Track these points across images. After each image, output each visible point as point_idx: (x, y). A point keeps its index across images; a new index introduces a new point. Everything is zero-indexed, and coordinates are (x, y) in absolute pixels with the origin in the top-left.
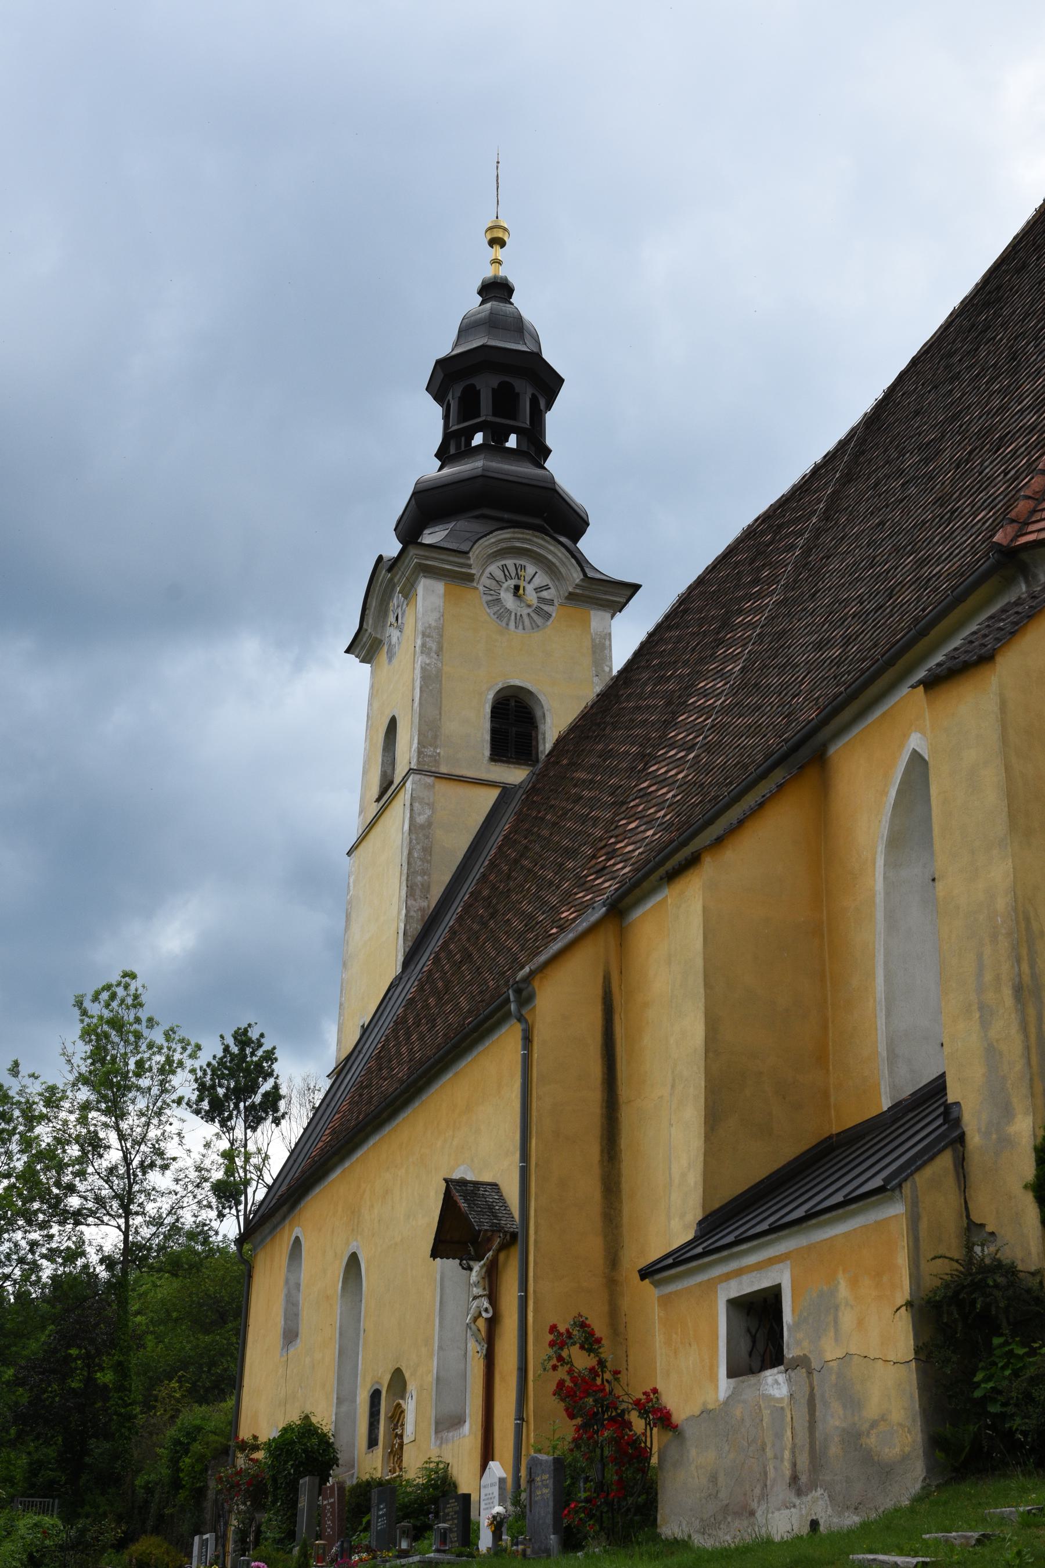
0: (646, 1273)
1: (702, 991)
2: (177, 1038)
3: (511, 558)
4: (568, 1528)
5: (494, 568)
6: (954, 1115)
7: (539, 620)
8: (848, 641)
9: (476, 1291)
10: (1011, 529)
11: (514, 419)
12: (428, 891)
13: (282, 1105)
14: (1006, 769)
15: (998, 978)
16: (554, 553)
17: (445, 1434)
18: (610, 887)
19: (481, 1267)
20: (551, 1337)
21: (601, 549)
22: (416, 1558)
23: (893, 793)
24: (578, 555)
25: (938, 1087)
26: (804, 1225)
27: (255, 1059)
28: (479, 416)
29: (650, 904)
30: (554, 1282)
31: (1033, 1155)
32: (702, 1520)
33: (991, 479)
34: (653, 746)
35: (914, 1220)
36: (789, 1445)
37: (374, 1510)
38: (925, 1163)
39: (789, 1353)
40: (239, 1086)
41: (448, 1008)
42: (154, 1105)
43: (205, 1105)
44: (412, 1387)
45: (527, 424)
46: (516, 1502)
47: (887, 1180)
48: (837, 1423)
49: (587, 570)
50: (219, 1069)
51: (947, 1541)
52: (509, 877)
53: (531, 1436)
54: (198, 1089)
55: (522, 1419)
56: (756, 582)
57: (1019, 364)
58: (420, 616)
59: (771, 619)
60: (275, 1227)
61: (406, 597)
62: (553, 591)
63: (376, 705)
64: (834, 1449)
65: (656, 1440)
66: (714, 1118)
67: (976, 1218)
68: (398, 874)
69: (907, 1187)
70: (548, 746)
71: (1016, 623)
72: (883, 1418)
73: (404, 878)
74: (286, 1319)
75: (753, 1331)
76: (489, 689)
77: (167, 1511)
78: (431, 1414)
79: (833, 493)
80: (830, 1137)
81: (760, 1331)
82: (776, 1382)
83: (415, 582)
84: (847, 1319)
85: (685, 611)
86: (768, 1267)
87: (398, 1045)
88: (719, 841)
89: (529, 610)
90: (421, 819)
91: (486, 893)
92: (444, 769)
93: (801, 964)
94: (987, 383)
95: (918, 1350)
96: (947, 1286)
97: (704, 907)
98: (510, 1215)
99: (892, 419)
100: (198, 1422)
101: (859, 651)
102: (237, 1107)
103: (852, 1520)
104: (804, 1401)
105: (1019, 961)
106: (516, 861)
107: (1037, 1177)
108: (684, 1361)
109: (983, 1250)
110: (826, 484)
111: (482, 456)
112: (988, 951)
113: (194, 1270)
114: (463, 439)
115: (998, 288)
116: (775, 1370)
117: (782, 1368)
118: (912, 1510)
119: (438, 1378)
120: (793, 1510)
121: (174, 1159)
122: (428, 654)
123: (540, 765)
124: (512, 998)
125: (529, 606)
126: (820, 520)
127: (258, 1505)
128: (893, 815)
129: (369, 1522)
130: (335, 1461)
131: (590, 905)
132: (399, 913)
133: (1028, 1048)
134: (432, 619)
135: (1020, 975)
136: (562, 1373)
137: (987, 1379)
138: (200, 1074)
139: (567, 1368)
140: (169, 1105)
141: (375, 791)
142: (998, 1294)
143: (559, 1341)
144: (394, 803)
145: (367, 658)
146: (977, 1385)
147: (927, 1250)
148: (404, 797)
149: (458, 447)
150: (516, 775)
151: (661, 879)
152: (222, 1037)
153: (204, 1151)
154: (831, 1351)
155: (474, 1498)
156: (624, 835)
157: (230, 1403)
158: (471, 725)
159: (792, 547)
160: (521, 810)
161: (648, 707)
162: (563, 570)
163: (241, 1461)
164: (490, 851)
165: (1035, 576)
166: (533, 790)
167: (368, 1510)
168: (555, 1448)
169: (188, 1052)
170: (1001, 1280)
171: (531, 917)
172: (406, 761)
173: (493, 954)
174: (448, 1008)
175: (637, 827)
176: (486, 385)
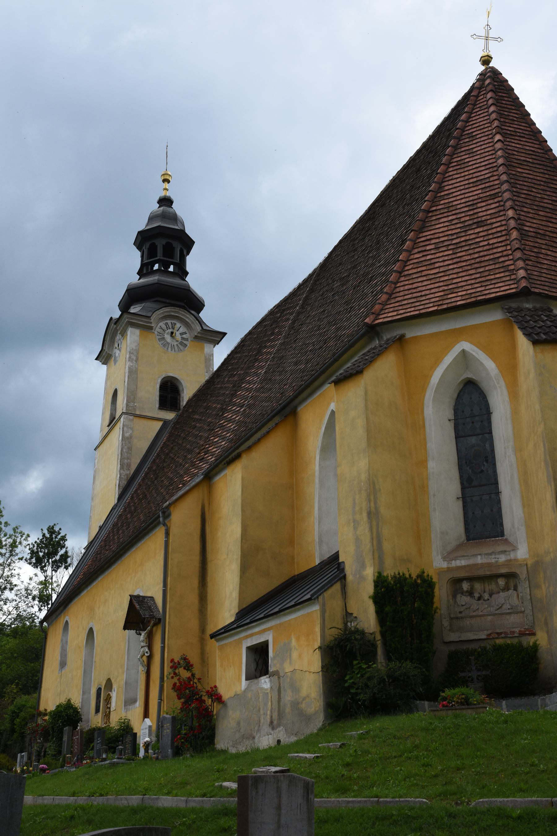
0: (213, 636)
1: (240, 513)
2: (19, 531)
3: (170, 320)
4: (177, 747)
5: (162, 324)
6: (342, 567)
7: (182, 347)
8: (308, 361)
9: (143, 644)
10: (372, 317)
11: (172, 258)
12: (130, 467)
13: (69, 560)
14: (367, 421)
15: (361, 509)
16: (189, 318)
17: (128, 707)
18: (205, 466)
19: (145, 634)
20: (171, 664)
21: (210, 317)
22: (108, 762)
23: (323, 428)
24: (199, 319)
25: (336, 556)
26: (279, 615)
27: (57, 540)
28: (157, 257)
29: (222, 474)
30: (177, 639)
31: (373, 584)
32: (233, 741)
33: (367, 294)
34: (226, 405)
35: (323, 612)
36: (270, 709)
37: (95, 741)
38: (328, 588)
39: (271, 670)
40: (49, 551)
41: (135, 519)
42: (7, 561)
43: (34, 560)
44: (115, 686)
45: (178, 261)
46: (158, 736)
47: (312, 596)
48: (289, 699)
49: (203, 326)
50: (40, 545)
51: (328, 746)
52: (164, 461)
53: (165, 707)
54: (30, 553)
55: (161, 700)
56: (272, 334)
57: (380, 246)
58: (128, 344)
59: (278, 350)
60: (57, 616)
61: (122, 336)
62: (188, 335)
63: (108, 384)
64: (288, 710)
65: (216, 708)
66: (244, 568)
67: (349, 611)
68: (116, 459)
69: (321, 598)
70: (185, 403)
71: (373, 357)
72: (308, 696)
73: (119, 461)
74: (61, 657)
75: (257, 660)
76: (159, 378)
77: (9, 743)
78: (123, 698)
79: (306, 297)
80: (294, 576)
81: (260, 660)
82: (265, 682)
83: (126, 329)
84: (295, 654)
85: (243, 346)
86: (263, 633)
87: (114, 535)
88: (250, 448)
89: (177, 343)
90: (127, 435)
91: (154, 468)
92: (138, 413)
93: (286, 496)
94: (368, 253)
95: (323, 667)
96: (335, 639)
97: (242, 477)
98: (158, 610)
99: (330, 266)
100: (23, 703)
101: (311, 366)
102: (48, 561)
103: (293, 739)
104: (276, 690)
105: (370, 501)
106: (167, 454)
107: (374, 593)
108: (229, 675)
109: (351, 625)
110: (303, 292)
111: (158, 274)
112: (357, 497)
113: (24, 635)
114: (150, 267)
115: (374, 213)
116: (265, 677)
117: (268, 676)
118: (317, 734)
119: (126, 683)
120: (270, 736)
121: (15, 585)
122: (132, 362)
123: (181, 412)
124: (161, 515)
125: (177, 341)
126: (300, 308)
127: (46, 740)
128: (324, 438)
129: (93, 746)
130: (80, 720)
131: (196, 475)
132: (117, 476)
133: (372, 539)
134: (134, 346)
135: (370, 507)
136: (175, 680)
137: (350, 679)
138: (31, 546)
139: (178, 677)
140: (14, 562)
141: (107, 422)
142: (356, 642)
143: (175, 666)
144: (116, 427)
145: (104, 363)
146: (346, 681)
147: (328, 625)
148: (120, 425)
149: (147, 270)
150: (170, 416)
151: (225, 464)
152: (42, 530)
153: (29, 582)
154: (288, 668)
155: (138, 735)
156: (213, 444)
157: (36, 695)
158: (151, 393)
159: (288, 320)
160: (171, 431)
161: (226, 387)
162: (192, 326)
163: (40, 721)
164: (158, 449)
165: (382, 337)
166: (177, 422)
167: (92, 742)
168: (174, 712)
169: (24, 538)
170: (358, 637)
171: (172, 479)
172: (121, 409)
173: (155, 495)
174: (135, 519)
175: (218, 440)
176: (160, 243)
